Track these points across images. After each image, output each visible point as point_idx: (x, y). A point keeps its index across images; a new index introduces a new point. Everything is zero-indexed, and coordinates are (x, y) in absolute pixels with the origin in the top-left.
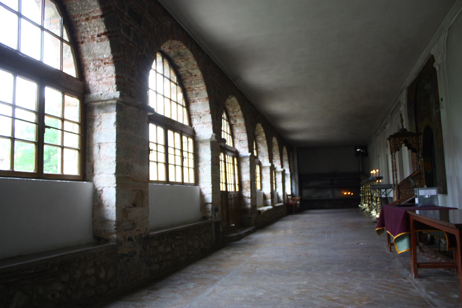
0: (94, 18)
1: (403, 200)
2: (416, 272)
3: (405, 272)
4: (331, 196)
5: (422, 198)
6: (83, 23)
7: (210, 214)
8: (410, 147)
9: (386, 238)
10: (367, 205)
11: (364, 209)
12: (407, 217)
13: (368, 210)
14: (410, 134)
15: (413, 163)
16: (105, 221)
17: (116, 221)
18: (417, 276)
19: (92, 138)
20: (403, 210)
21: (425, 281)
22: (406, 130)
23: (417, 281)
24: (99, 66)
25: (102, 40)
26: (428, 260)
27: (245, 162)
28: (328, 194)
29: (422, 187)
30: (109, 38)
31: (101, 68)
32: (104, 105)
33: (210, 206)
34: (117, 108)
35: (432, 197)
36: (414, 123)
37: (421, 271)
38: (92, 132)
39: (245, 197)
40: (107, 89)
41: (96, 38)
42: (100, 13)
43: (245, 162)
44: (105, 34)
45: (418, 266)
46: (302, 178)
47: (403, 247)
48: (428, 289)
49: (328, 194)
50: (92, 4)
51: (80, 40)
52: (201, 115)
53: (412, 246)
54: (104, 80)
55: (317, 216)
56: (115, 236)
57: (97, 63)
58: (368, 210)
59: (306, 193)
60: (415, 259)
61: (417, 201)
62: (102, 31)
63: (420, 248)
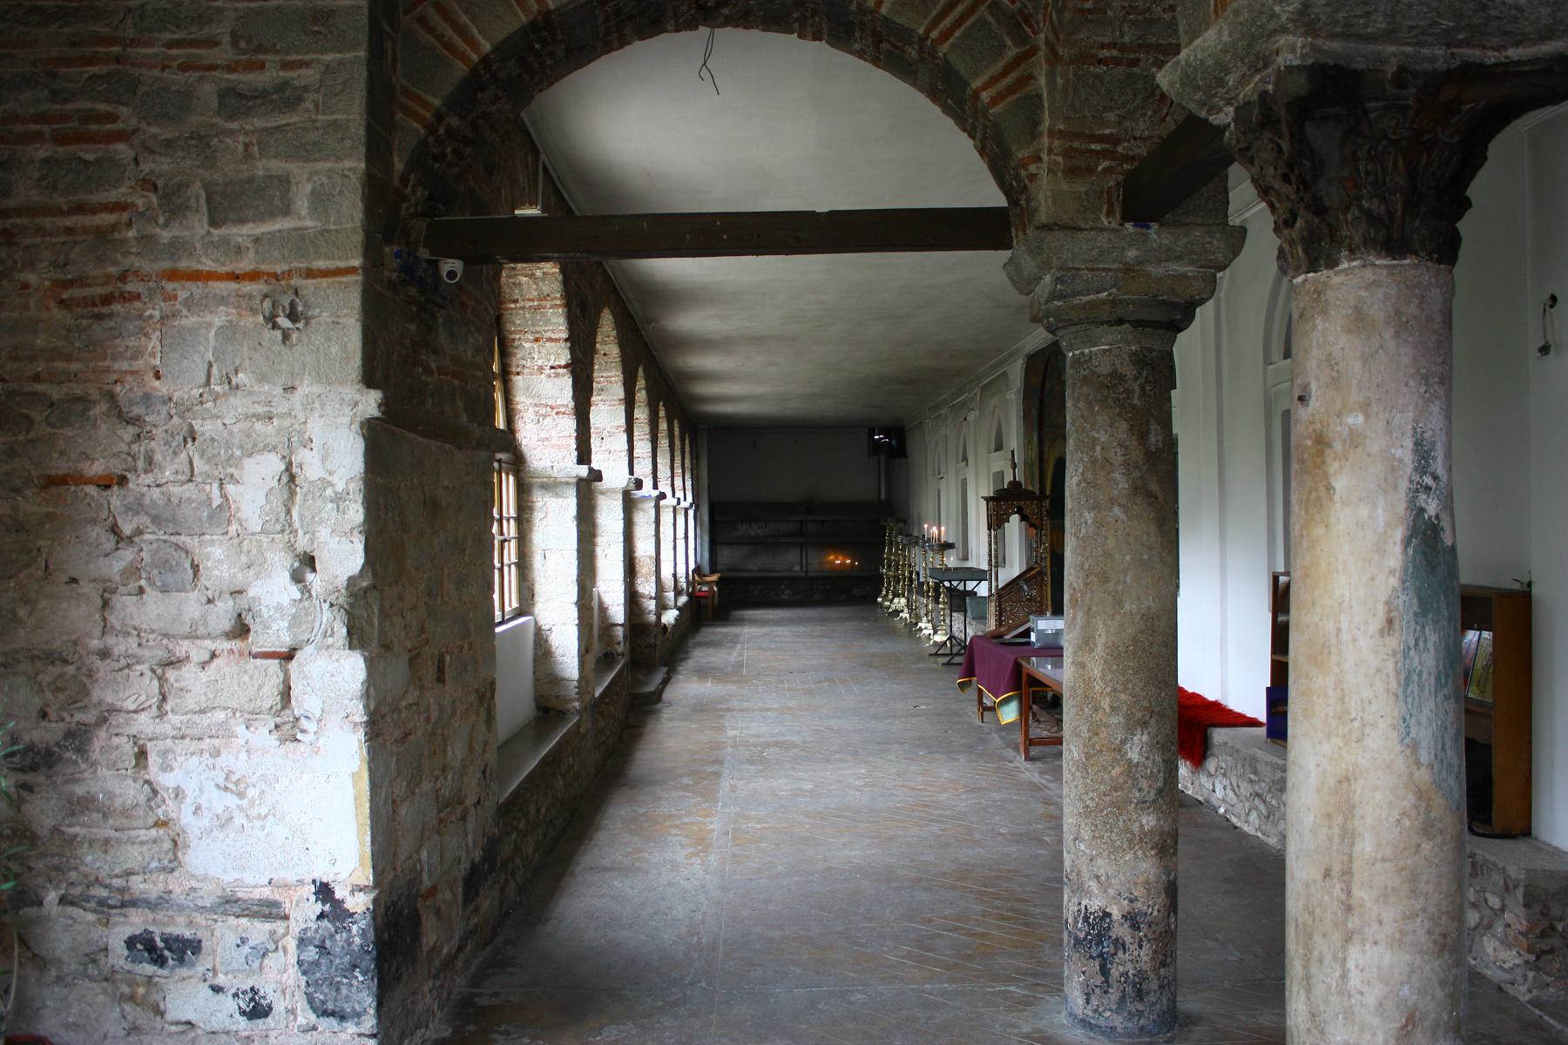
0: (550, 340)
1: (1010, 629)
2: (1027, 752)
3: (1010, 753)
4: (797, 568)
5: (1040, 633)
6: (527, 345)
7: (620, 649)
8: (1023, 518)
9: (975, 696)
10: (903, 601)
11: (897, 612)
12: (1018, 668)
13: (905, 615)
14: (1029, 495)
15: (1030, 549)
16: (556, 680)
17: (579, 681)
18: (1028, 758)
19: (531, 541)
20: (1010, 655)
21: (1039, 764)
22: (1019, 484)
23: (1028, 765)
24: (545, 416)
25: (557, 375)
26: (1045, 734)
27: (643, 510)
28: (789, 561)
29: (1041, 613)
30: (573, 373)
31: (548, 419)
32: (552, 486)
33: (620, 632)
34: (578, 491)
35: (1058, 633)
36: (1035, 439)
37: (1034, 751)
38: (531, 530)
39: (642, 596)
40: (560, 457)
41: (548, 371)
42: (565, 335)
43: (643, 510)
44: (565, 367)
45: (1030, 742)
46: (721, 518)
47: (1010, 713)
48: (1042, 773)
49: (789, 561)
50: (554, 320)
51: (514, 370)
52: (605, 434)
53: (1024, 712)
54: (554, 442)
55: (779, 630)
56: (577, 704)
57: (543, 411)
58: (905, 615)
59: (727, 556)
60: (1027, 733)
61: (1033, 637)
62: (563, 363)
63: (1034, 715)
